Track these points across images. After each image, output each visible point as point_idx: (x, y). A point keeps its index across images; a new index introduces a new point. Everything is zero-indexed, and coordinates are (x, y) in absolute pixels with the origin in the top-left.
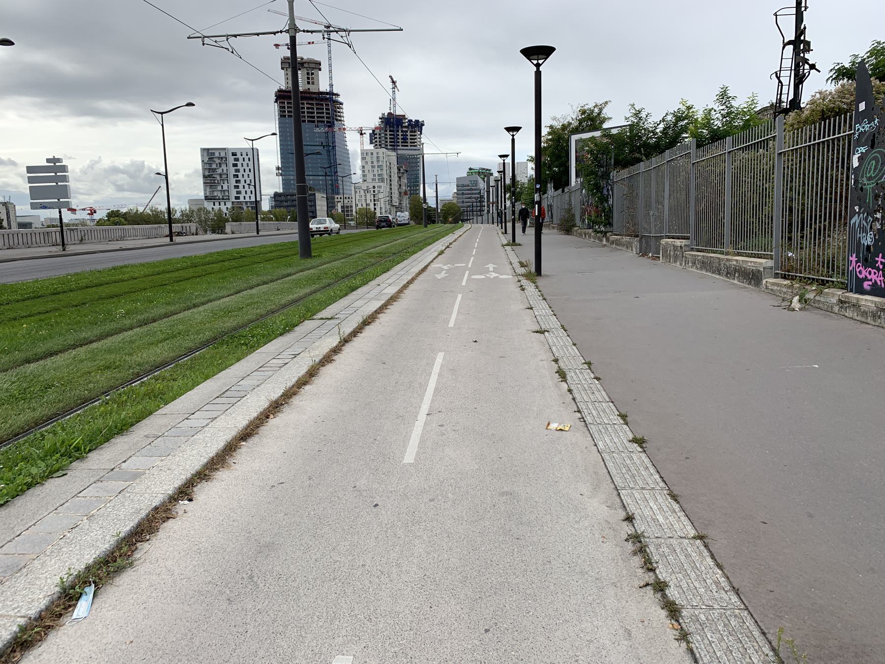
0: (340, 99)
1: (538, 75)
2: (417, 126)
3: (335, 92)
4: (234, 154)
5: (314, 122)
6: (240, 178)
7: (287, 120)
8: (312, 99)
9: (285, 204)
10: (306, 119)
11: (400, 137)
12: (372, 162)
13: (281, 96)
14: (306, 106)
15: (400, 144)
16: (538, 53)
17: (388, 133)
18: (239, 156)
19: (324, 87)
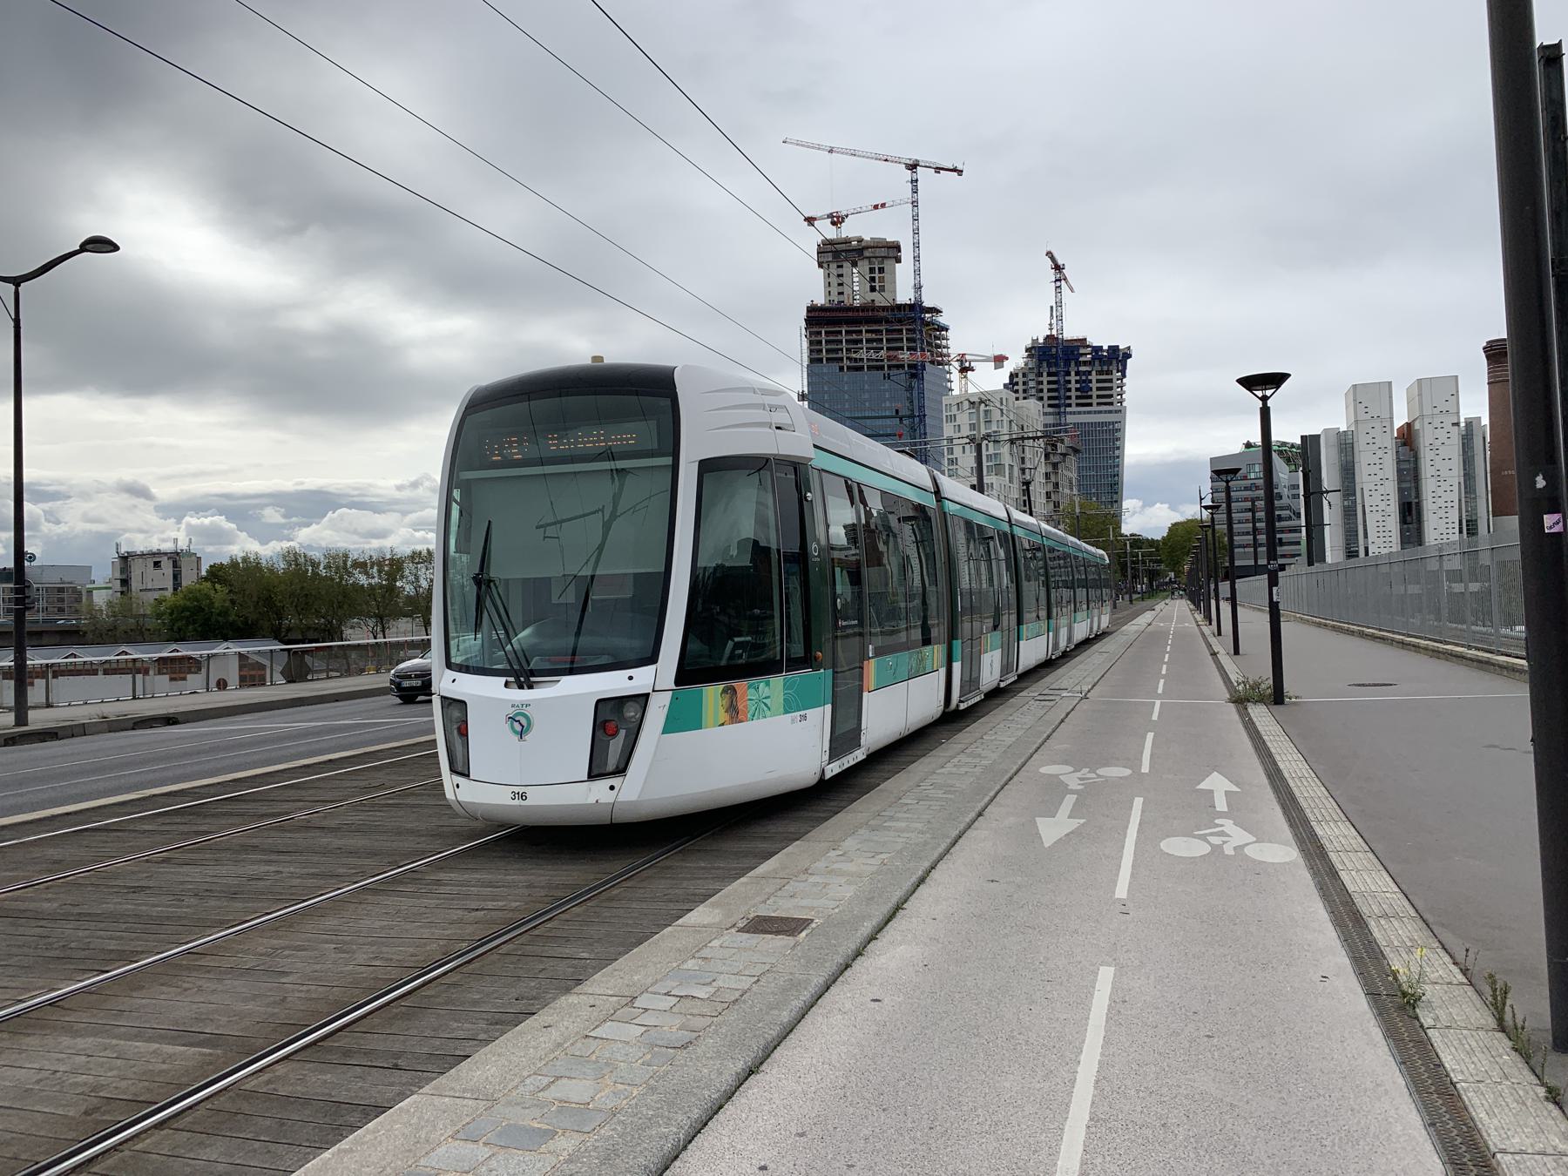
0: (942, 320)
1: (1265, 414)
2: (1116, 359)
5: (882, 368)
7: (825, 368)
8: (878, 321)
11: (1073, 386)
13: (817, 318)
14: (865, 336)
15: (1073, 401)
16: (1263, 383)
17: (1045, 379)
19: (904, 296)
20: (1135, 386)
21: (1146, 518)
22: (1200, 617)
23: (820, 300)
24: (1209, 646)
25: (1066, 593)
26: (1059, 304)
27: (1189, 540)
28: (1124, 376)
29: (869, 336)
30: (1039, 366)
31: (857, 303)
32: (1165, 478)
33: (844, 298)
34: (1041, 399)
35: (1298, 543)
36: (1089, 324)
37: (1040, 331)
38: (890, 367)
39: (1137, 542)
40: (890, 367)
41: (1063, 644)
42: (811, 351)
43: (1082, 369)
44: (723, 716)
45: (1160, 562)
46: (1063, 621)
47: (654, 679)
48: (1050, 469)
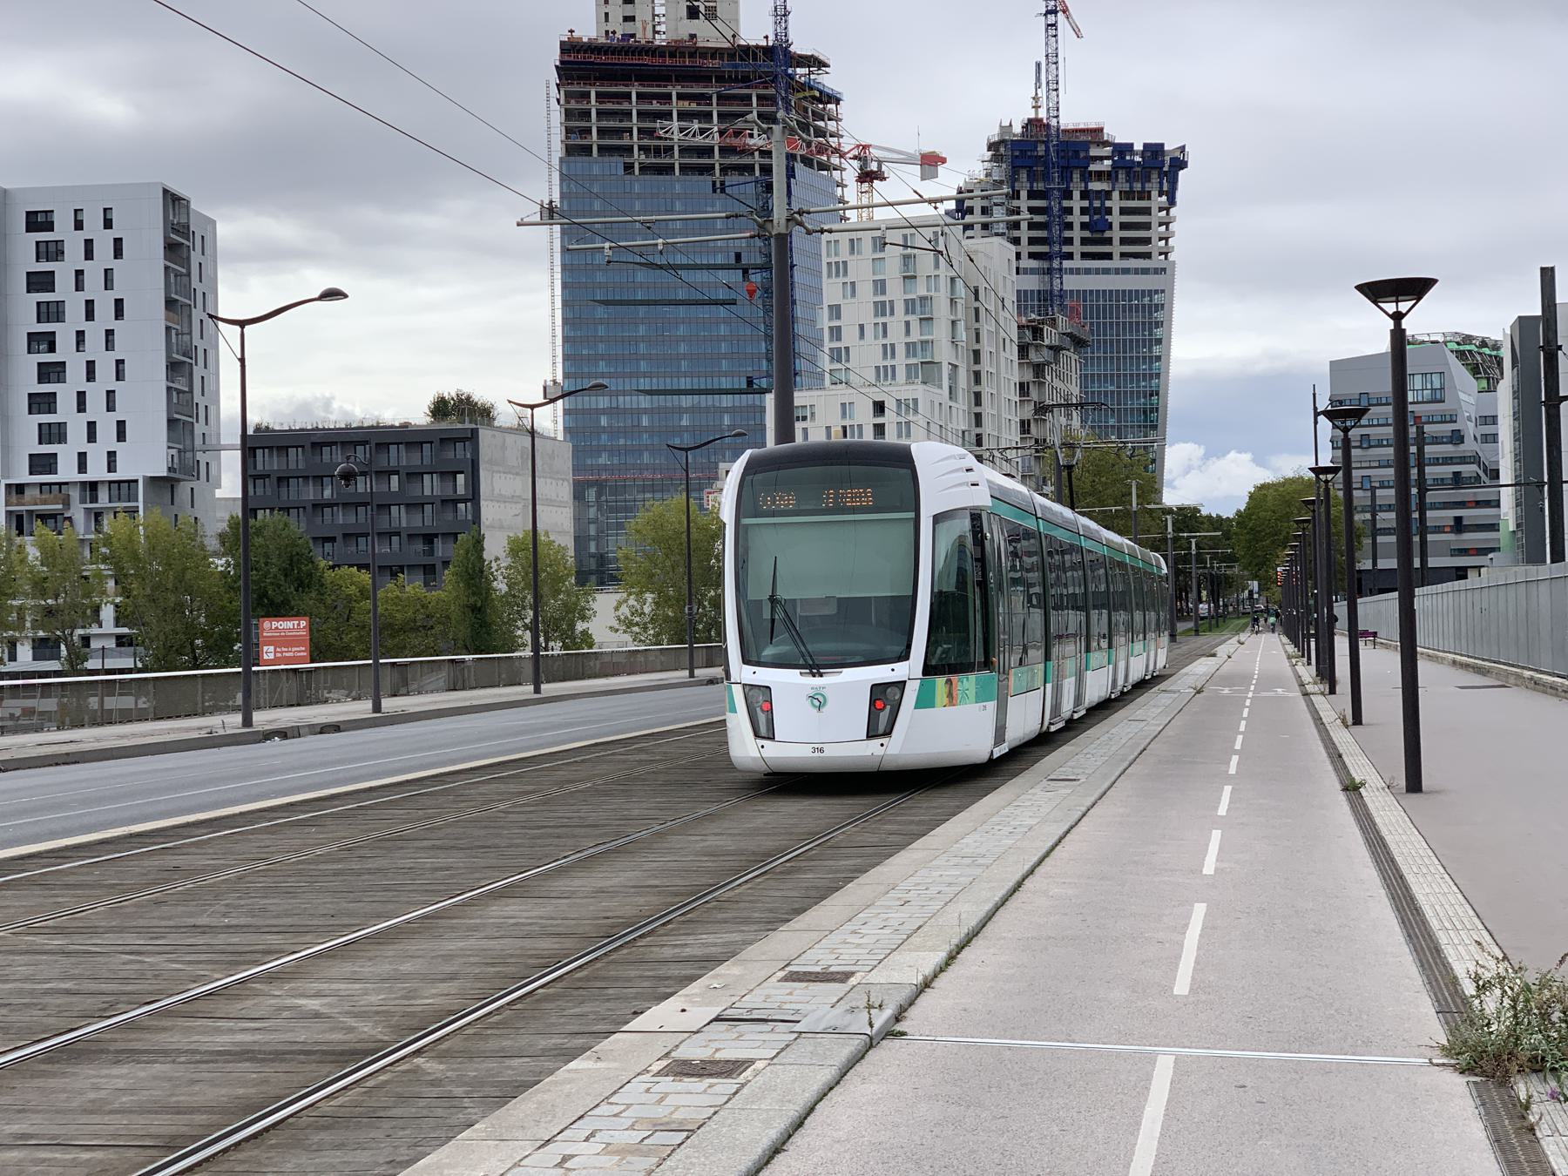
0: (828, 81)
2: (1156, 169)
3: (798, 48)
4: (38, 221)
6: (65, 351)
7: (597, 165)
8: (702, 77)
9: (310, 493)
10: (677, 159)
11: (1077, 218)
12: (880, 286)
15: (1077, 248)
18: (63, 229)
20: (1194, 225)
21: (1207, 476)
22: (1308, 672)
23: (588, 31)
24: (1336, 758)
25: (1073, 618)
26: (1053, 58)
27: (1287, 517)
28: (1172, 202)
29: (686, 105)
30: (1013, 179)
31: (660, 40)
32: (1241, 405)
33: (635, 28)
34: (1016, 241)
35: (1493, 527)
36: (1108, 99)
37: (1017, 115)
38: (725, 170)
39: (1188, 518)
40: (725, 170)
41: (1067, 707)
42: (569, 131)
43: (1095, 186)
44: (946, 700)
45: (1230, 559)
46: (1122, 653)
47: (909, 670)
48: (1029, 376)
